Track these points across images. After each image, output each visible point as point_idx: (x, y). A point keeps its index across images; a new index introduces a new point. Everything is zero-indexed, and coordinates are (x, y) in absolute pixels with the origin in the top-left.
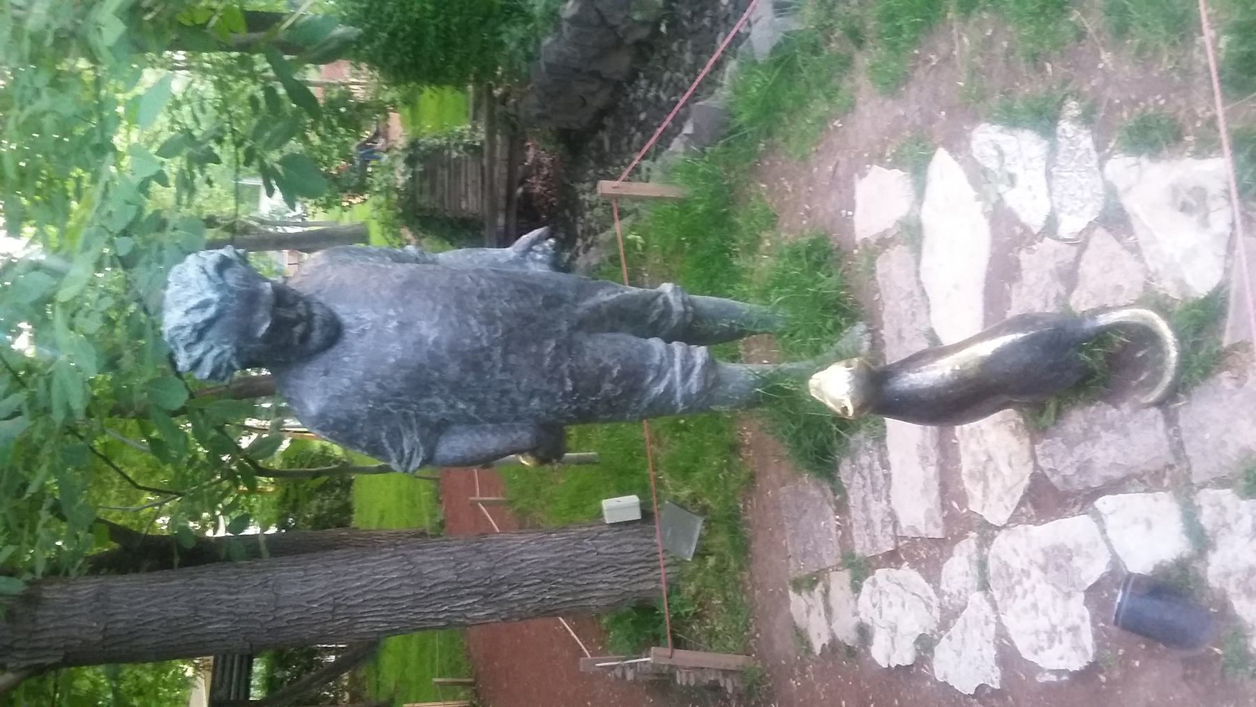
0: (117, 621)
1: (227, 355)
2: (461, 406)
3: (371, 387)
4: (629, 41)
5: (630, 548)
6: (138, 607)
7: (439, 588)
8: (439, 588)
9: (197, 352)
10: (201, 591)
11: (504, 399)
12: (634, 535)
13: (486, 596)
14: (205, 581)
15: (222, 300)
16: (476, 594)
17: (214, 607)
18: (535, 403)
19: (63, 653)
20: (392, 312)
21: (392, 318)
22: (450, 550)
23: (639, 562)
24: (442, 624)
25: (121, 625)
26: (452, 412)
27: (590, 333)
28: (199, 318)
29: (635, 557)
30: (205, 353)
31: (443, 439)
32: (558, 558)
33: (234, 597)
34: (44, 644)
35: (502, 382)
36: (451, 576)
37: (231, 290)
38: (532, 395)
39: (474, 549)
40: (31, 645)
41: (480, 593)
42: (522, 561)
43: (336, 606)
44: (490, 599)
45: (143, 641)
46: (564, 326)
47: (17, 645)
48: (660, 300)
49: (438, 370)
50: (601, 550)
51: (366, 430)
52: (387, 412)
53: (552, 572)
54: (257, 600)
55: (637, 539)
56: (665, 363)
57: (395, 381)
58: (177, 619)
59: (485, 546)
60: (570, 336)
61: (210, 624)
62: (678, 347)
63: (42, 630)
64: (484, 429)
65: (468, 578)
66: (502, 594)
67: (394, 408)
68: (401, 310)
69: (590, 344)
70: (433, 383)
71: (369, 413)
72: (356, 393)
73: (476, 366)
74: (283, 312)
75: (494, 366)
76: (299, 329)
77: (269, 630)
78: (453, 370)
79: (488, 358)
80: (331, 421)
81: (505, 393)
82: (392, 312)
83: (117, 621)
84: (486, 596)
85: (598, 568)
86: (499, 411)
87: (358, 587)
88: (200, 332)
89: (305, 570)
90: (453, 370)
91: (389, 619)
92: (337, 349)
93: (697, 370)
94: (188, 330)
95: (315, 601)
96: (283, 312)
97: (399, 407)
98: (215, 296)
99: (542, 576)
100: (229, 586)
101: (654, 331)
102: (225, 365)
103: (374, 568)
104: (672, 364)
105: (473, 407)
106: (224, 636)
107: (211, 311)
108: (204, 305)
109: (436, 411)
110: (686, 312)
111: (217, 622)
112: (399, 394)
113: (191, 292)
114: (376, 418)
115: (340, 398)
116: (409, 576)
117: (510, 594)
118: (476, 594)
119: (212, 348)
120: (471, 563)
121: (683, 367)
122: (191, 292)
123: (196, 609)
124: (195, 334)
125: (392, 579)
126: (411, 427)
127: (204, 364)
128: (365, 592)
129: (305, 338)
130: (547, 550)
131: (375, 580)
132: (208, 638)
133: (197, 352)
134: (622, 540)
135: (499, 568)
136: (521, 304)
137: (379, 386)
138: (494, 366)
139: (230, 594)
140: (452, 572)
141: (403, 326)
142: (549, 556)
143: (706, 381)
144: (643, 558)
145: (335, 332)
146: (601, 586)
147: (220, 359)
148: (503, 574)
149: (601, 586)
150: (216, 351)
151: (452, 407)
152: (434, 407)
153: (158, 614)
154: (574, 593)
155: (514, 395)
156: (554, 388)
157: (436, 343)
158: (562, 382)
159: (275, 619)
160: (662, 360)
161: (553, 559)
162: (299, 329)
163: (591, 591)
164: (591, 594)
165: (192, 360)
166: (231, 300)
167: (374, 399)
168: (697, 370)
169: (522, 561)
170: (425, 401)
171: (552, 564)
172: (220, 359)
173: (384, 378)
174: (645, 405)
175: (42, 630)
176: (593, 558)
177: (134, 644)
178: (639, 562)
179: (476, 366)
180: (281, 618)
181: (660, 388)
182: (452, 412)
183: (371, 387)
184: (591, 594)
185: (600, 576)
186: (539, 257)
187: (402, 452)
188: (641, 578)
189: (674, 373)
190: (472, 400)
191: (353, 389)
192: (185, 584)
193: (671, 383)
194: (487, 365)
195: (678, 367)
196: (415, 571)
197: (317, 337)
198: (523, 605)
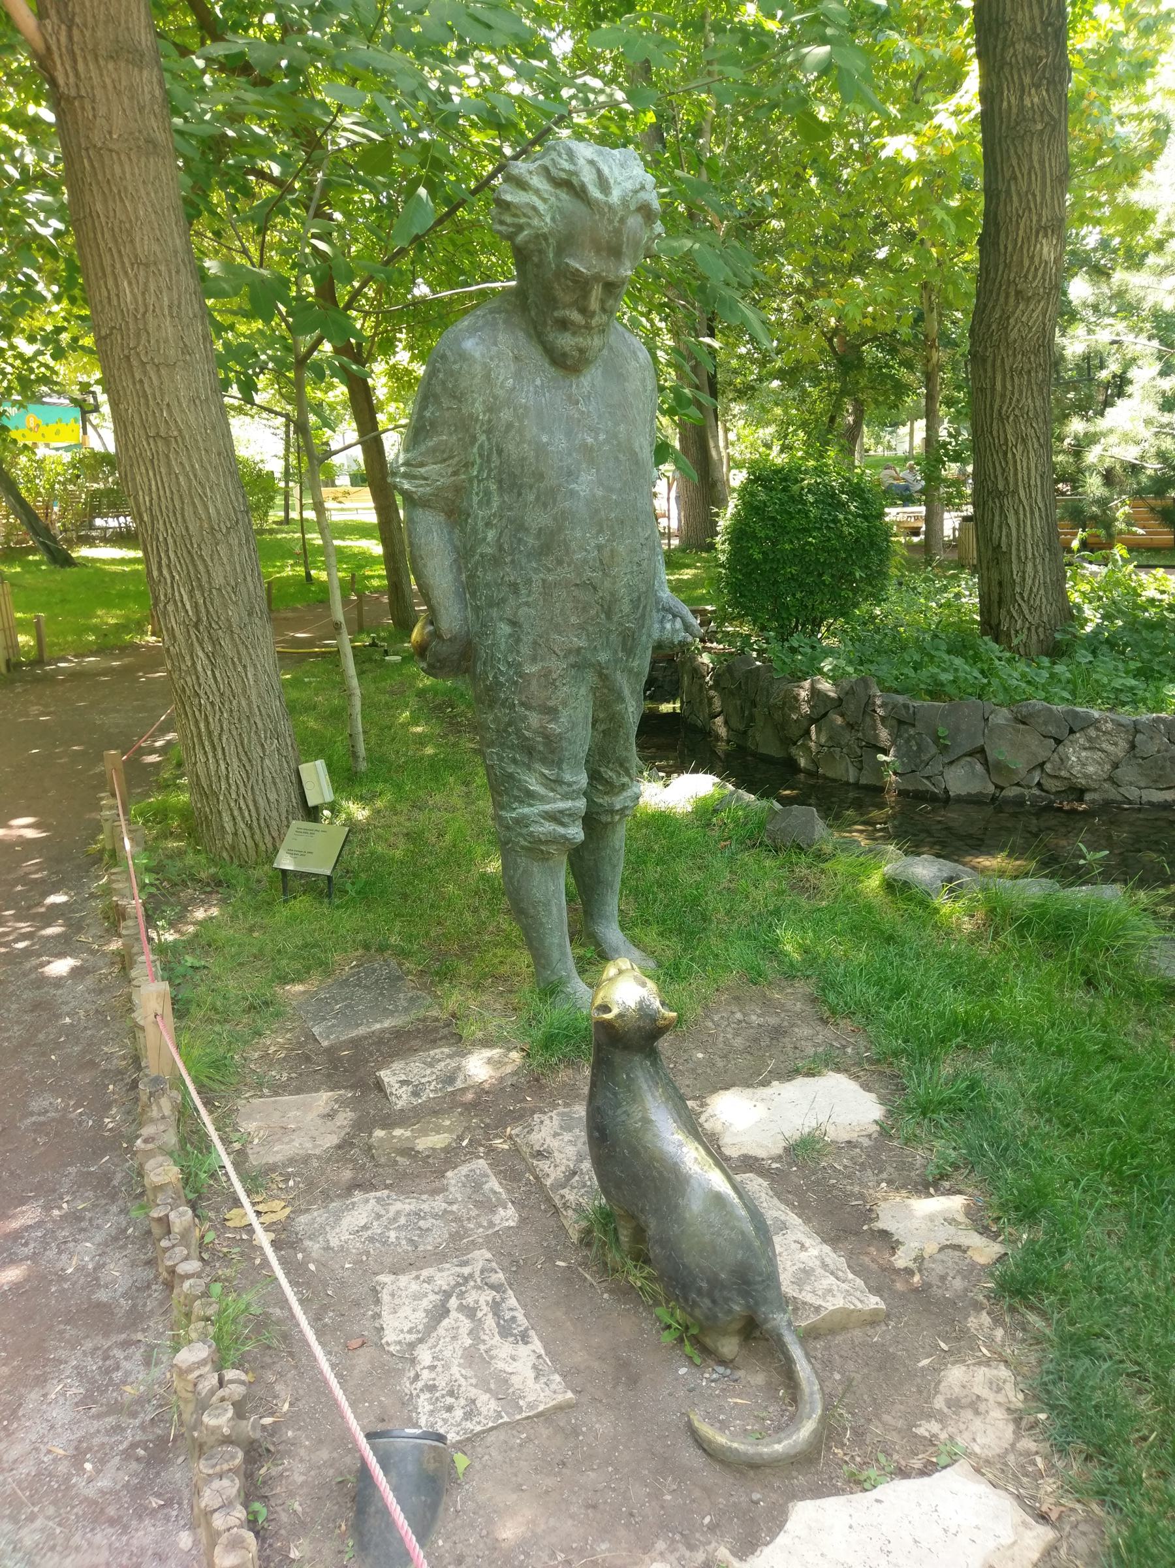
0: (121, 165)
1: (536, 222)
2: (491, 535)
3: (506, 415)
4: (793, 750)
5: (273, 797)
6: (143, 192)
7: (201, 568)
8: (201, 568)
9: (537, 181)
10: (170, 272)
11: (505, 588)
12: (289, 799)
13: (196, 626)
14: (183, 278)
15: (610, 207)
16: (197, 613)
17: (152, 287)
18: (505, 629)
19: (73, 93)
20: (602, 437)
21: (596, 439)
22: (249, 579)
23: (257, 809)
24: (155, 574)
25: (117, 170)
26: (480, 524)
27: (594, 690)
28: (588, 177)
29: (262, 803)
30: (537, 192)
31: (442, 517)
32: (250, 708)
33: (166, 312)
34: (81, 67)
35: (529, 582)
36: (219, 580)
37: (622, 221)
38: (513, 623)
39: (252, 608)
40: (78, 52)
41: (199, 620)
42: (245, 667)
43: (166, 440)
44: (192, 631)
45: (99, 197)
46: (603, 657)
47: (75, 32)
48: (626, 780)
49: (538, 498)
50: (267, 761)
51: (447, 414)
52: (474, 439)
53: (235, 702)
54: (166, 341)
55: (284, 804)
56: (565, 788)
57: (518, 444)
58: (132, 241)
59: (257, 620)
60: (592, 665)
61: (130, 283)
62: (581, 804)
63: (99, 67)
64: (459, 570)
65: (217, 602)
66: (201, 644)
67: (481, 447)
68: (606, 448)
69: (583, 691)
70: (520, 494)
71: (471, 416)
72: (495, 398)
73: (545, 549)
74: (597, 292)
75: (549, 570)
76: (576, 316)
77: (128, 358)
78: (537, 519)
79: (560, 562)
80: (456, 367)
81: (514, 588)
82: (602, 437)
83: (121, 165)
84: (196, 626)
85: (244, 758)
86: (488, 585)
87: (193, 466)
88: (569, 185)
89: (207, 399)
90: (537, 519)
91: (155, 508)
92: (552, 371)
93: (561, 830)
94: (566, 165)
95: (170, 413)
96: (597, 292)
97: (481, 456)
98: (615, 196)
99: (228, 692)
100: (179, 307)
101: (595, 776)
102: (522, 220)
103: (218, 485)
104: (565, 797)
105: (489, 550)
106: (115, 303)
107: (595, 193)
108: (603, 184)
109: (480, 502)
110: (612, 812)
111: (132, 292)
112: (500, 452)
113: (616, 171)
114: (464, 425)
115: (487, 378)
116: (213, 528)
117: (201, 654)
118: (197, 613)
119: (545, 200)
120: (235, 603)
121: (561, 812)
122: (616, 171)
123: (147, 265)
124: (564, 176)
125: (206, 508)
126: (455, 473)
127: (522, 193)
128: (187, 476)
129: (564, 325)
130: (260, 696)
131: (203, 487)
132: (110, 283)
133: (537, 181)
134: (280, 785)
135: (232, 639)
136: (626, 600)
137: (509, 426)
138: (549, 570)
139: (170, 307)
140: (222, 581)
141: (587, 450)
142: (254, 698)
143: (547, 842)
144: (262, 813)
145: (567, 364)
146: (223, 767)
147: (531, 213)
148: (226, 643)
149: (223, 767)
150: (541, 206)
151: (488, 524)
152: (486, 501)
153: (137, 218)
154: (210, 733)
155: (512, 601)
156: (525, 649)
157: (572, 493)
158: (534, 659)
159: (143, 364)
160: (569, 785)
161: (250, 704)
162: (576, 316)
163: (215, 756)
164: (210, 755)
165: (527, 177)
166: (611, 221)
167: (490, 421)
168: (561, 830)
169: (245, 667)
170: (494, 487)
171: (244, 703)
172: (531, 213)
173: (520, 431)
174: (511, 769)
175: (99, 67)
176: (257, 752)
177: (95, 188)
178: (257, 809)
179: (545, 549)
180: (145, 373)
181: (535, 786)
182: (480, 524)
183: (506, 415)
184: (210, 755)
185: (235, 763)
186: (668, 626)
187: (422, 465)
188: (236, 813)
189: (555, 801)
190: (501, 548)
191: (501, 393)
192: (176, 252)
193: (543, 799)
194: (549, 562)
195: (562, 805)
196: (219, 536)
197: (566, 341)
198: (188, 672)
